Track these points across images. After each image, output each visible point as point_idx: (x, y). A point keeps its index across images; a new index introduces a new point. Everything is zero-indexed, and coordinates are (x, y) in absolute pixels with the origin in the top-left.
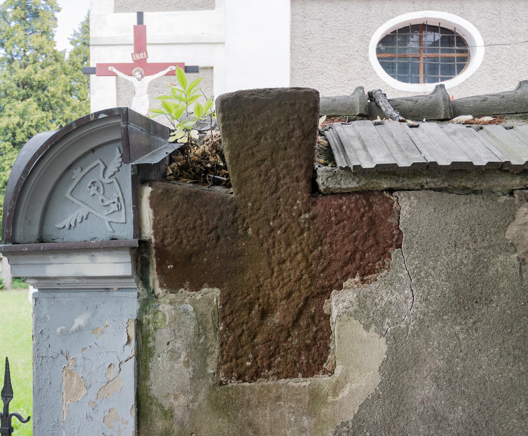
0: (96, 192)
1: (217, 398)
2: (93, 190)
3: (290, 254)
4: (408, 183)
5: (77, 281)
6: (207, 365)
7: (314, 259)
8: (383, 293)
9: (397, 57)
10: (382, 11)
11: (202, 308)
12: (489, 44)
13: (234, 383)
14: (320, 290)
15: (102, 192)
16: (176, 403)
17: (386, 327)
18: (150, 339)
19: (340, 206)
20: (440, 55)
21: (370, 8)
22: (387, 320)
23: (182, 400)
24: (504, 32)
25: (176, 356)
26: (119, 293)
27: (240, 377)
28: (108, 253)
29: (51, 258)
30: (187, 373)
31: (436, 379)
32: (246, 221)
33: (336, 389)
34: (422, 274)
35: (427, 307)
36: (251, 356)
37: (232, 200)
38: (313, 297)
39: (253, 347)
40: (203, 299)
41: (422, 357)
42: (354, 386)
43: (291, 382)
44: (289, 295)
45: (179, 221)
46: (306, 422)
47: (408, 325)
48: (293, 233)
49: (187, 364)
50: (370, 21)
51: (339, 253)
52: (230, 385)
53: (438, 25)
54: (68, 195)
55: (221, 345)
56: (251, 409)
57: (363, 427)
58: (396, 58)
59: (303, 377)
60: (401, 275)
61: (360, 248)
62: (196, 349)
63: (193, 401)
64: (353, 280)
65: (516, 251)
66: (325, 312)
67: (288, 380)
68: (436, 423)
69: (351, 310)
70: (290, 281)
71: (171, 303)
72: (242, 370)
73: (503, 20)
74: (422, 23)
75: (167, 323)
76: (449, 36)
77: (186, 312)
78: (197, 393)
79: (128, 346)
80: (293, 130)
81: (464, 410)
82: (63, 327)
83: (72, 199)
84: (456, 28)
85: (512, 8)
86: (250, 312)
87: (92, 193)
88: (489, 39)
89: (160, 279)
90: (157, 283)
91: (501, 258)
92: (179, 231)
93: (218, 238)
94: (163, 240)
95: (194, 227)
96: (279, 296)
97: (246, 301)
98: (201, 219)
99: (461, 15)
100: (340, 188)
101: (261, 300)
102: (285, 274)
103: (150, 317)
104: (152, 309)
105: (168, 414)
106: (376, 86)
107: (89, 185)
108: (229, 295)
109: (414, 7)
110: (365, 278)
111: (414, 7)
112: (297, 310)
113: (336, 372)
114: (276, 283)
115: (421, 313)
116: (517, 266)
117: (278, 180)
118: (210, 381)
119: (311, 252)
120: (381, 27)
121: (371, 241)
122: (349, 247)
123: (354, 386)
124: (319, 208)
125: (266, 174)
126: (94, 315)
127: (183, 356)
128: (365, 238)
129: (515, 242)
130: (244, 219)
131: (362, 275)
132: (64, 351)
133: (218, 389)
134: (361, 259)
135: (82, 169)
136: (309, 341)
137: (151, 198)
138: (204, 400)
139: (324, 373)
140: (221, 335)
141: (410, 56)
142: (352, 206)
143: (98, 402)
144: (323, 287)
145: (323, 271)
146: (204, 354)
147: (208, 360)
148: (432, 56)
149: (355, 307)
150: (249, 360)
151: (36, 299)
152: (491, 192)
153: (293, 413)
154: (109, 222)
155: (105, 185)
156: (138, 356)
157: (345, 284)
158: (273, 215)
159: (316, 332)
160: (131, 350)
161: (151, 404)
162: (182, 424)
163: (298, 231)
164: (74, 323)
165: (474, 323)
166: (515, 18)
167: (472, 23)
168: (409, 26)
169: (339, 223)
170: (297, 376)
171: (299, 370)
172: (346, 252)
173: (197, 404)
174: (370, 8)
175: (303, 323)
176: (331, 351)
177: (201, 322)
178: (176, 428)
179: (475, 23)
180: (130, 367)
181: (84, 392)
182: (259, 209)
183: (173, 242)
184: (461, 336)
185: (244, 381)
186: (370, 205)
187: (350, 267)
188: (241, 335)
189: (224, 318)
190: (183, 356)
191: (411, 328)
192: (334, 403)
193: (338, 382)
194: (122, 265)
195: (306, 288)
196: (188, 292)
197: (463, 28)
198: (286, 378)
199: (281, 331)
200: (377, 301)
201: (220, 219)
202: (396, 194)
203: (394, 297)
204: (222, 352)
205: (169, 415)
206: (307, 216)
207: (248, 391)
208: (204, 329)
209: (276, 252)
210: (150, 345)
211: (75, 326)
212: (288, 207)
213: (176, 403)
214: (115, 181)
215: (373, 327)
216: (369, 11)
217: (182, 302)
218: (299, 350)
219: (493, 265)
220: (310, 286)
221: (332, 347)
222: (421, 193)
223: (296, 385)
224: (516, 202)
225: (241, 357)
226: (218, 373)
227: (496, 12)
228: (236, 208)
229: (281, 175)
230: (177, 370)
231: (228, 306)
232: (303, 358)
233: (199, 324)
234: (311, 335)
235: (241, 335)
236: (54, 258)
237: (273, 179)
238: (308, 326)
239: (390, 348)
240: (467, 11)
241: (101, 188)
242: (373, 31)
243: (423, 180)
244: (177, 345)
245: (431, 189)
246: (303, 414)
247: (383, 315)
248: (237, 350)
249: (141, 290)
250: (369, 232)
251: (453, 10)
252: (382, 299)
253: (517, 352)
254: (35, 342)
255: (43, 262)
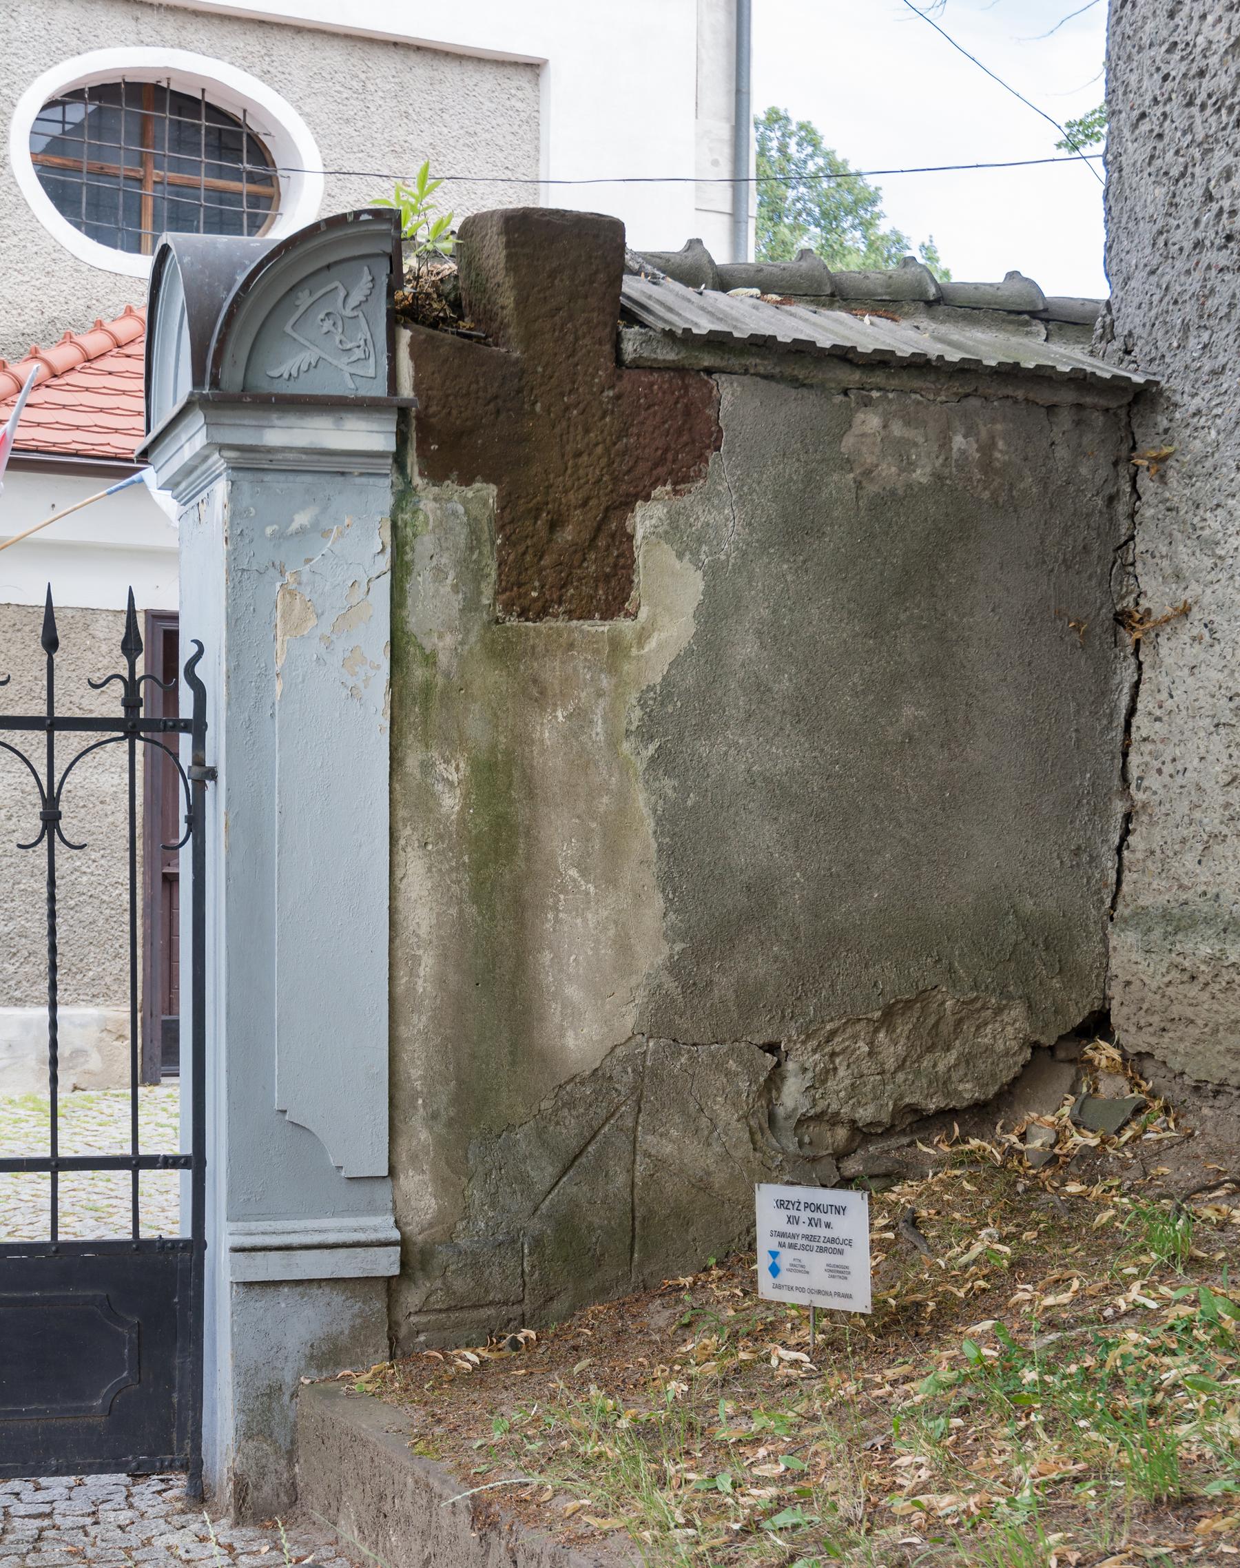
0: (332, 329)
1: (493, 641)
2: (328, 325)
3: (588, 444)
4: (734, 362)
5: (304, 457)
6: (482, 593)
7: (617, 455)
8: (699, 509)
9: (85, 170)
10: (48, 27)
11: (476, 510)
12: (337, 169)
13: (512, 622)
14: (623, 499)
15: (340, 330)
16: (441, 644)
17: (703, 557)
18: (408, 549)
19: (652, 384)
20: (204, 180)
21: (14, 14)
22: (704, 548)
23: (449, 640)
24: (375, 142)
25: (442, 575)
26: (364, 480)
27: (523, 614)
28: (378, 416)
29: (275, 419)
30: (457, 602)
31: (759, 633)
32: (535, 392)
33: (642, 637)
34: (745, 489)
35: (751, 534)
36: (537, 584)
37: (517, 360)
38: (615, 508)
39: (540, 571)
40: (476, 497)
41: (744, 602)
42: (663, 635)
43: (586, 625)
44: (585, 503)
45: (448, 383)
46: (605, 682)
47: (728, 556)
48: (593, 416)
49: (455, 589)
50: (13, 50)
51: (647, 450)
52: (508, 624)
53: (200, 97)
54: (288, 329)
55: (500, 565)
56: (536, 659)
57: (673, 694)
58: (81, 172)
59: (601, 619)
60: (720, 488)
61: (673, 446)
62: (467, 568)
63: (462, 643)
64: (663, 489)
65: (851, 470)
66: (629, 530)
67: (581, 622)
68: (758, 695)
69: (660, 530)
70: (587, 482)
71: (435, 500)
72: (526, 602)
73: (373, 109)
74: (153, 81)
75: (430, 527)
76: (220, 129)
77: (454, 513)
78: (467, 631)
79: (381, 556)
80: (597, 272)
81: (790, 680)
82: (275, 527)
83: (295, 335)
84: (249, 110)
85: (397, 80)
86: (535, 523)
87: (325, 330)
88: (335, 156)
89: (419, 463)
90: (416, 469)
91: (836, 477)
92: (448, 396)
93: (498, 412)
94: (427, 407)
95: (468, 394)
96: (573, 502)
97: (531, 505)
98: (478, 383)
99: (265, 76)
100: (655, 360)
101: (550, 506)
102: (581, 472)
103: (407, 516)
104: (410, 506)
105: (430, 660)
106: (29, 245)
107: (322, 316)
108: (510, 494)
109: (139, 33)
110: (678, 488)
111: (139, 33)
112: (595, 524)
113: (640, 615)
114: (569, 484)
115: (744, 541)
116: (854, 491)
117: (577, 339)
118: (485, 616)
119: (615, 444)
120: (45, 75)
121: (685, 438)
122: (660, 442)
123: (663, 635)
124: (624, 385)
125: (561, 329)
126: (324, 510)
127: (450, 577)
128: (680, 432)
129: (852, 458)
130: (532, 389)
131: (675, 484)
132: (277, 563)
133: (495, 628)
134: (674, 461)
135: (311, 293)
136: (608, 570)
137: (412, 345)
138: (476, 643)
139: (626, 616)
140: (499, 551)
141: (122, 173)
142: (666, 386)
143: (334, 637)
144: (628, 495)
145: (629, 471)
146: (478, 576)
147: (483, 585)
148: (178, 181)
149: (666, 527)
150: (534, 589)
151: (233, 483)
152: (822, 387)
153: (589, 668)
154: (351, 375)
155: (346, 320)
156: (393, 569)
157: (655, 493)
158: (568, 388)
159: (618, 556)
160: (385, 562)
161: (408, 643)
162: (447, 675)
163: (599, 413)
164: (292, 520)
165: (804, 562)
166: (403, 108)
167: (292, 102)
168: (118, 84)
169: (649, 408)
170: (592, 618)
171: (597, 610)
172: (657, 449)
173: (467, 647)
174: (14, 14)
175: (601, 543)
176: (635, 585)
177: (474, 532)
178: (440, 680)
179: (300, 104)
180: (383, 586)
181: (313, 622)
182: (551, 377)
183: (439, 412)
184: (789, 578)
185: (527, 620)
186: (686, 388)
187: (661, 471)
188: (524, 553)
189: (502, 528)
190: (450, 577)
191: (732, 561)
192: (638, 658)
193: (643, 628)
194: (382, 436)
195: (606, 495)
196: (456, 487)
197: (270, 115)
198: (579, 619)
199: (575, 552)
200: (692, 520)
201: (502, 385)
202: (715, 376)
203: (712, 517)
204: (500, 575)
205: (431, 661)
206: (611, 393)
207: (532, 634)
208: (478, 539)
209: (571, 439)
210: (408, 557)
211: (295, 526)
212: (588, 379)
213: (441, 644)
214: (361, 315)
215: (688, 556)
216: (11, 21)
217: (449, 500)
218: (597, 580)
219: (827, 485)
220: (612, 491)
221: (636, 581)
222: (746, 379)
223: (593, 630)
224: (853, 405)
225: (525, 584)
226: (494, 605)
227: (354, 83)
228: (523, 371)
229: (580, 333)
230: (443, 596)
231: (508, 510)
232: (601, 592)
233: (472, 532)
234: (611, 560)
235: (524, 553)
236: (279, 418)
237: (571, 338)
238: (608, 548)
239: (707, 586)
240: (280, 69)
241: (340, 323)
242: (22, 84)
243: (751, 361)
244: (443, 561)
245: (757, 375)
246: (601, 670)
247: (700, 541)
248: (520, 574)
249: (394, 477)
250: (684, 424)
251: (244, 58)
252: (698, 518)
253: (852, 605)
254: (230, 548)
255: (261, 423)
